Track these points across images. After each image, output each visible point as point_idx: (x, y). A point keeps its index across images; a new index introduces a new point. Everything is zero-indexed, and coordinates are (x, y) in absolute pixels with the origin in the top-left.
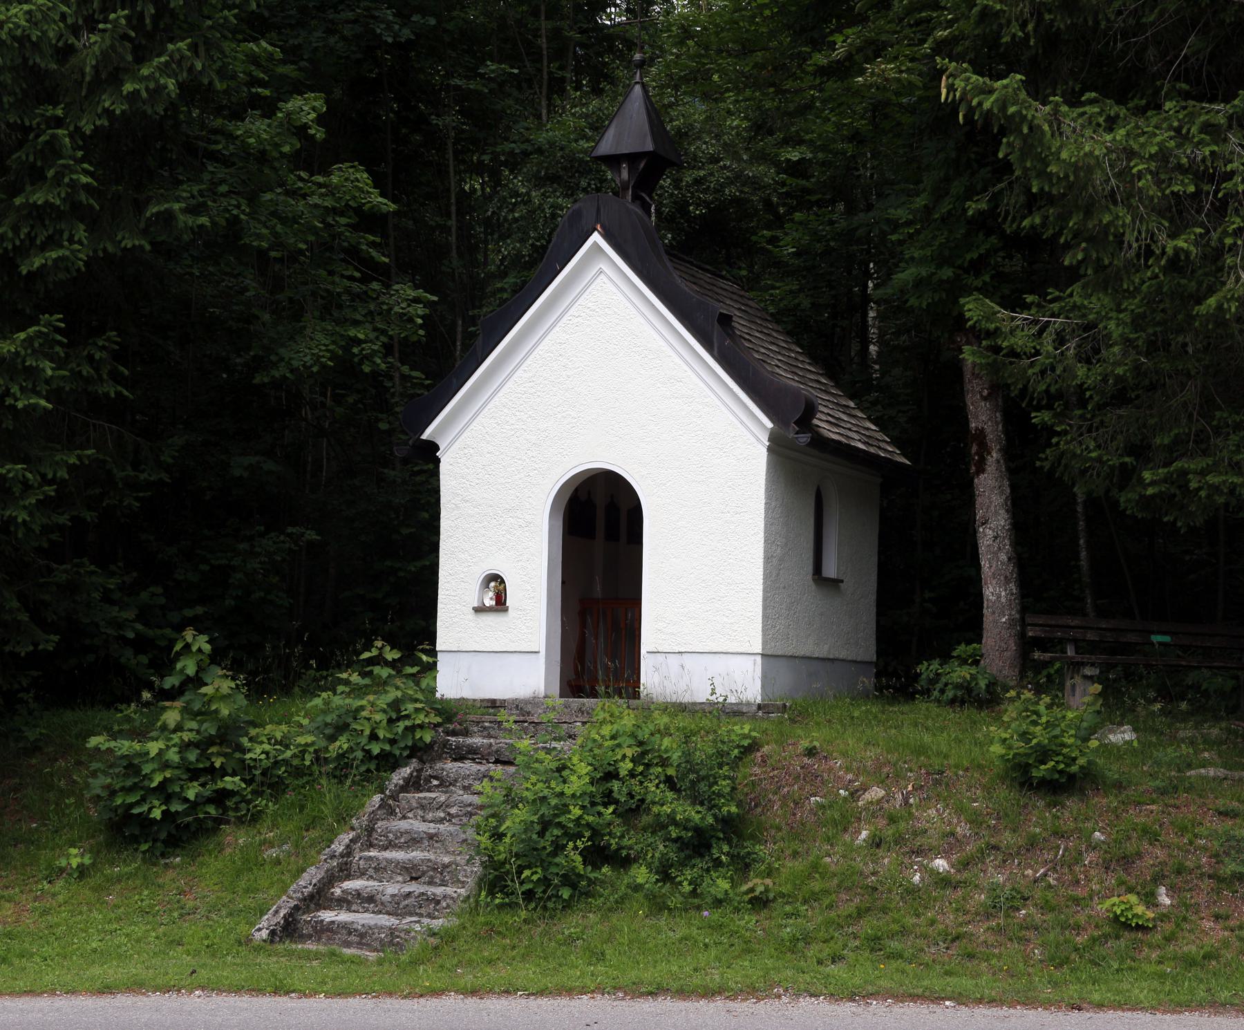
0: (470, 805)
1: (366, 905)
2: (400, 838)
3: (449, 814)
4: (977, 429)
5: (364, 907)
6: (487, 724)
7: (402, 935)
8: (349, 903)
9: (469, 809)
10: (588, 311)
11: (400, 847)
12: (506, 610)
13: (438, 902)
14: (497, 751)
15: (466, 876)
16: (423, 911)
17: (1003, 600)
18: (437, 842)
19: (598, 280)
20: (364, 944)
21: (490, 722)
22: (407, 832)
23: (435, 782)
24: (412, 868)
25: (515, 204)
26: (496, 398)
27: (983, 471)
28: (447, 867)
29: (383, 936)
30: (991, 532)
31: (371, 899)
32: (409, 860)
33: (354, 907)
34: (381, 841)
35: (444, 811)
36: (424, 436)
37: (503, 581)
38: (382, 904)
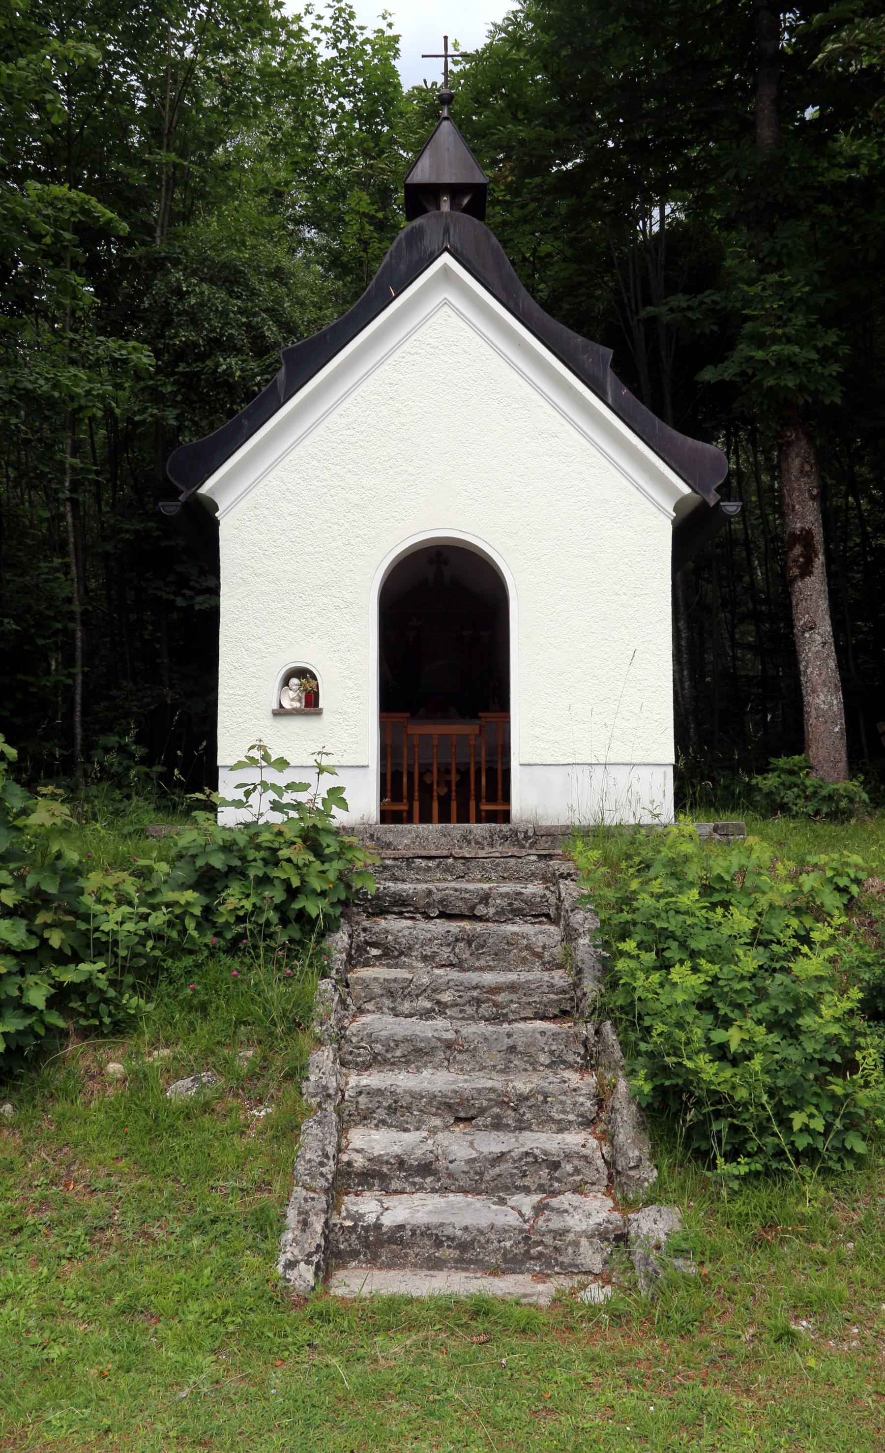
0: (475, 988)
1: (417, 1180)
2: (393, 1050)
3: (438, 1003)
4: (802, 529)
5: (414, 1184)
6: (388, 862)
7: (548, 1240)
8: (384, 1178)
9: (475, 994)
10: (428, 348)
11: (393, 1064)
12: (319, 713)
13: (555, 1166)
14: (441, 901)
15: (564, 1112)
16: (527, 1182)
17: (835, 709)
18: (460, 1052)
19: (441, 313)
20: (471, 1261)
21: (395, 859)
22: (406, 1040)
23: (375, 952)
24: (459, 1104)
25: (281, 237)
26: (300, 448)
27: (810, 573)
28: (527, 1099)
29: (508, 1244)
30: (819, 638)
31: (426, 1169)
32: (455, 1092)
33: (395, 1185)
34: (359, 1055)
35: (428, 998)
36: (204, 490)
37: (314, 677)
38: (450, 1175)
